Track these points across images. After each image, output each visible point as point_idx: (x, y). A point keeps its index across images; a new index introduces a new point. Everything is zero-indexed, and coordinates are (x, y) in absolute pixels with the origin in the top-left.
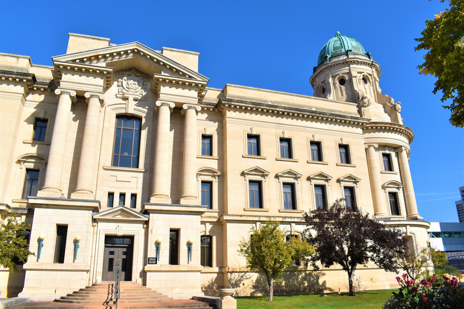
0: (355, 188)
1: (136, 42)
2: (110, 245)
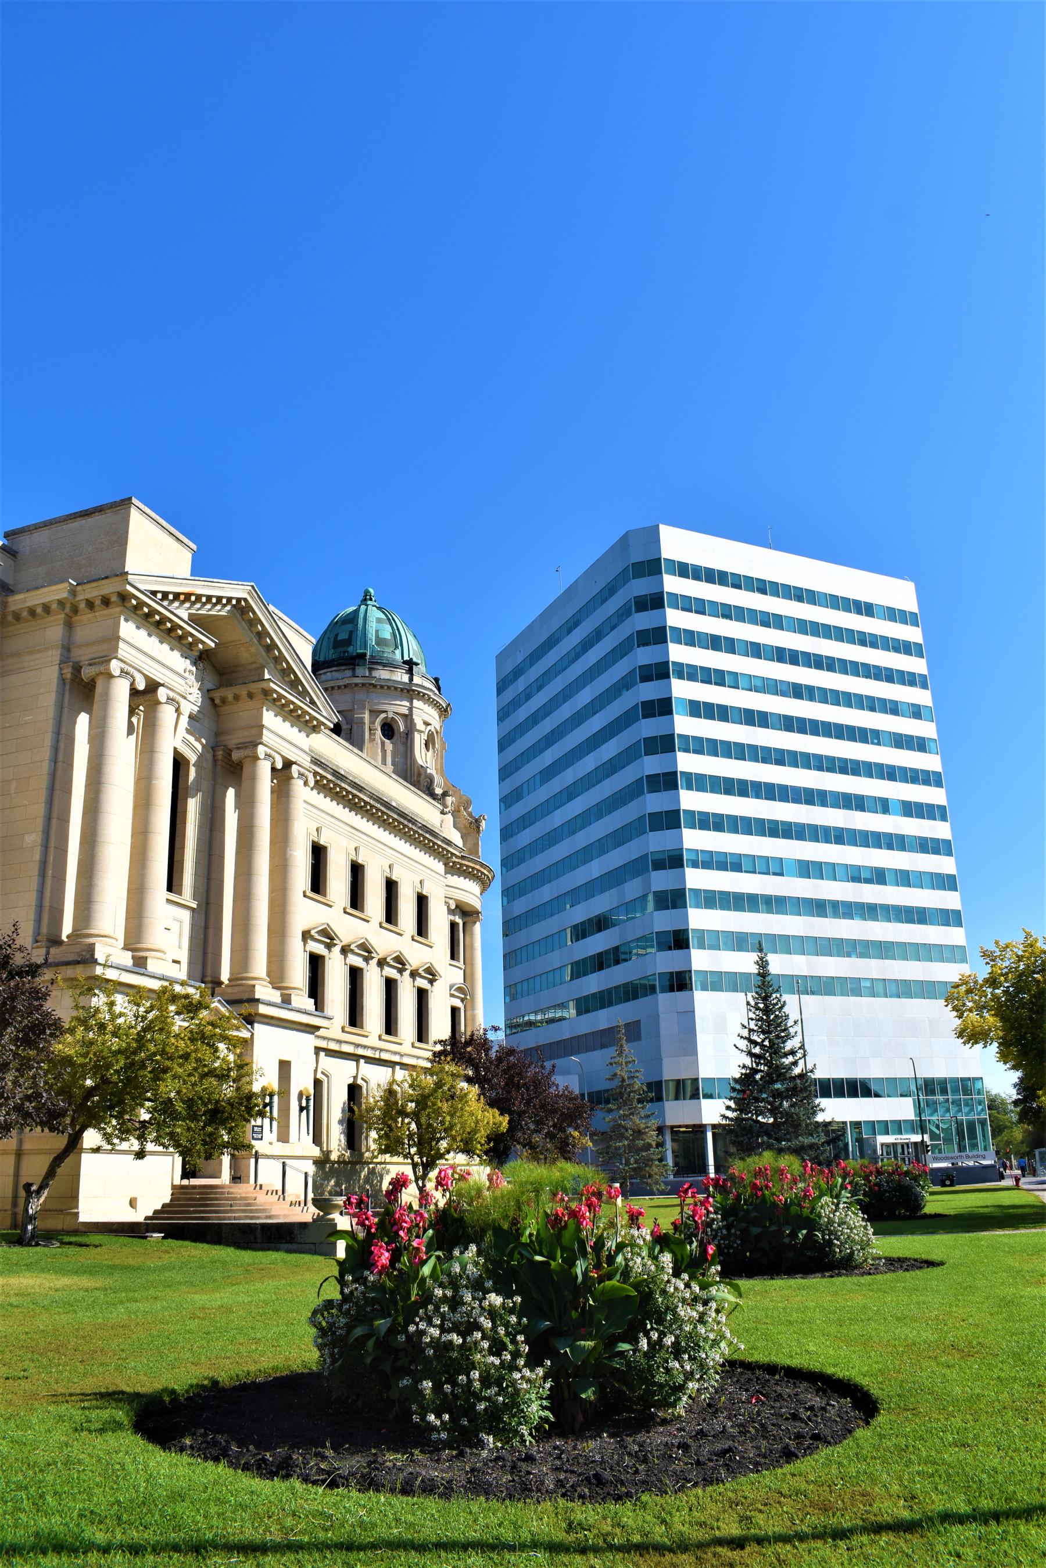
0: (399, 982)
1: (249, 584)
2: (681, 1129)
